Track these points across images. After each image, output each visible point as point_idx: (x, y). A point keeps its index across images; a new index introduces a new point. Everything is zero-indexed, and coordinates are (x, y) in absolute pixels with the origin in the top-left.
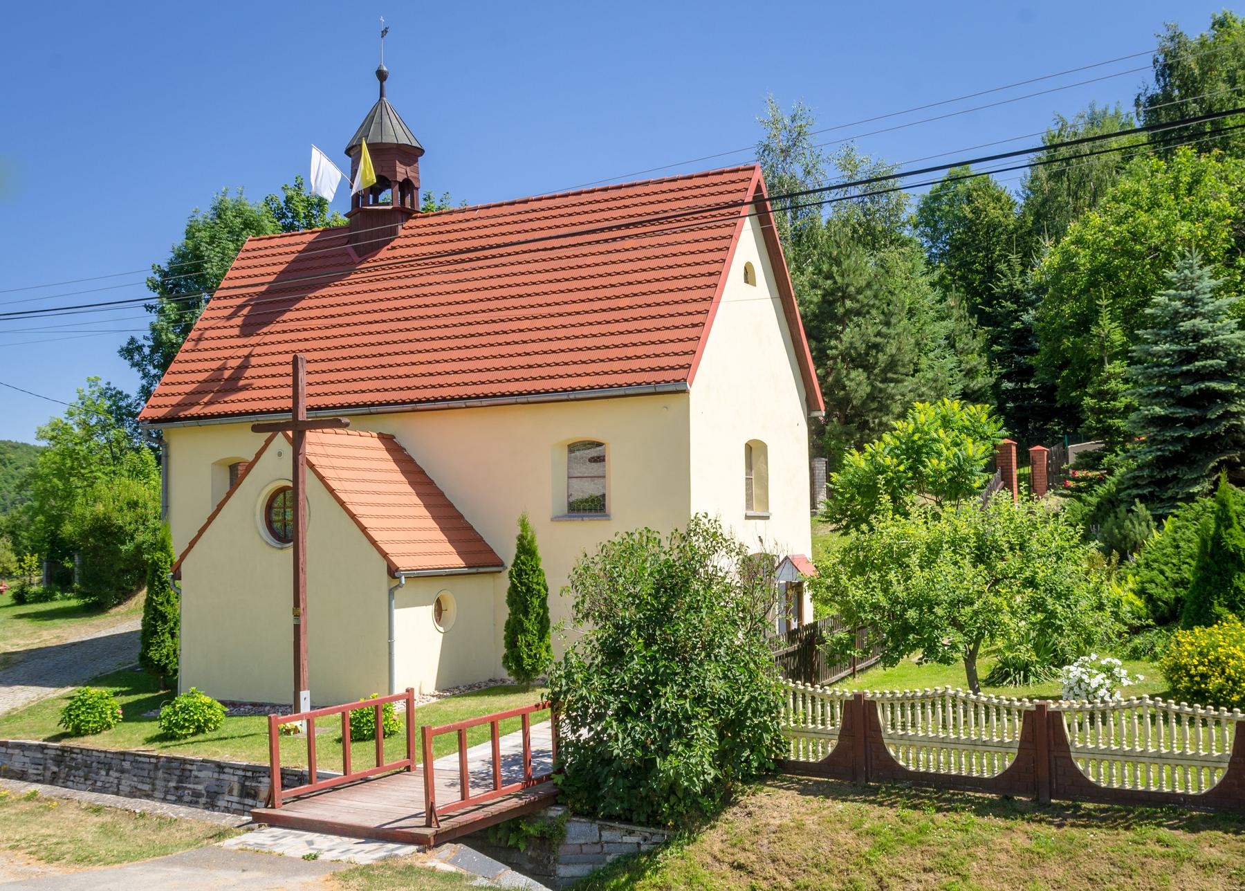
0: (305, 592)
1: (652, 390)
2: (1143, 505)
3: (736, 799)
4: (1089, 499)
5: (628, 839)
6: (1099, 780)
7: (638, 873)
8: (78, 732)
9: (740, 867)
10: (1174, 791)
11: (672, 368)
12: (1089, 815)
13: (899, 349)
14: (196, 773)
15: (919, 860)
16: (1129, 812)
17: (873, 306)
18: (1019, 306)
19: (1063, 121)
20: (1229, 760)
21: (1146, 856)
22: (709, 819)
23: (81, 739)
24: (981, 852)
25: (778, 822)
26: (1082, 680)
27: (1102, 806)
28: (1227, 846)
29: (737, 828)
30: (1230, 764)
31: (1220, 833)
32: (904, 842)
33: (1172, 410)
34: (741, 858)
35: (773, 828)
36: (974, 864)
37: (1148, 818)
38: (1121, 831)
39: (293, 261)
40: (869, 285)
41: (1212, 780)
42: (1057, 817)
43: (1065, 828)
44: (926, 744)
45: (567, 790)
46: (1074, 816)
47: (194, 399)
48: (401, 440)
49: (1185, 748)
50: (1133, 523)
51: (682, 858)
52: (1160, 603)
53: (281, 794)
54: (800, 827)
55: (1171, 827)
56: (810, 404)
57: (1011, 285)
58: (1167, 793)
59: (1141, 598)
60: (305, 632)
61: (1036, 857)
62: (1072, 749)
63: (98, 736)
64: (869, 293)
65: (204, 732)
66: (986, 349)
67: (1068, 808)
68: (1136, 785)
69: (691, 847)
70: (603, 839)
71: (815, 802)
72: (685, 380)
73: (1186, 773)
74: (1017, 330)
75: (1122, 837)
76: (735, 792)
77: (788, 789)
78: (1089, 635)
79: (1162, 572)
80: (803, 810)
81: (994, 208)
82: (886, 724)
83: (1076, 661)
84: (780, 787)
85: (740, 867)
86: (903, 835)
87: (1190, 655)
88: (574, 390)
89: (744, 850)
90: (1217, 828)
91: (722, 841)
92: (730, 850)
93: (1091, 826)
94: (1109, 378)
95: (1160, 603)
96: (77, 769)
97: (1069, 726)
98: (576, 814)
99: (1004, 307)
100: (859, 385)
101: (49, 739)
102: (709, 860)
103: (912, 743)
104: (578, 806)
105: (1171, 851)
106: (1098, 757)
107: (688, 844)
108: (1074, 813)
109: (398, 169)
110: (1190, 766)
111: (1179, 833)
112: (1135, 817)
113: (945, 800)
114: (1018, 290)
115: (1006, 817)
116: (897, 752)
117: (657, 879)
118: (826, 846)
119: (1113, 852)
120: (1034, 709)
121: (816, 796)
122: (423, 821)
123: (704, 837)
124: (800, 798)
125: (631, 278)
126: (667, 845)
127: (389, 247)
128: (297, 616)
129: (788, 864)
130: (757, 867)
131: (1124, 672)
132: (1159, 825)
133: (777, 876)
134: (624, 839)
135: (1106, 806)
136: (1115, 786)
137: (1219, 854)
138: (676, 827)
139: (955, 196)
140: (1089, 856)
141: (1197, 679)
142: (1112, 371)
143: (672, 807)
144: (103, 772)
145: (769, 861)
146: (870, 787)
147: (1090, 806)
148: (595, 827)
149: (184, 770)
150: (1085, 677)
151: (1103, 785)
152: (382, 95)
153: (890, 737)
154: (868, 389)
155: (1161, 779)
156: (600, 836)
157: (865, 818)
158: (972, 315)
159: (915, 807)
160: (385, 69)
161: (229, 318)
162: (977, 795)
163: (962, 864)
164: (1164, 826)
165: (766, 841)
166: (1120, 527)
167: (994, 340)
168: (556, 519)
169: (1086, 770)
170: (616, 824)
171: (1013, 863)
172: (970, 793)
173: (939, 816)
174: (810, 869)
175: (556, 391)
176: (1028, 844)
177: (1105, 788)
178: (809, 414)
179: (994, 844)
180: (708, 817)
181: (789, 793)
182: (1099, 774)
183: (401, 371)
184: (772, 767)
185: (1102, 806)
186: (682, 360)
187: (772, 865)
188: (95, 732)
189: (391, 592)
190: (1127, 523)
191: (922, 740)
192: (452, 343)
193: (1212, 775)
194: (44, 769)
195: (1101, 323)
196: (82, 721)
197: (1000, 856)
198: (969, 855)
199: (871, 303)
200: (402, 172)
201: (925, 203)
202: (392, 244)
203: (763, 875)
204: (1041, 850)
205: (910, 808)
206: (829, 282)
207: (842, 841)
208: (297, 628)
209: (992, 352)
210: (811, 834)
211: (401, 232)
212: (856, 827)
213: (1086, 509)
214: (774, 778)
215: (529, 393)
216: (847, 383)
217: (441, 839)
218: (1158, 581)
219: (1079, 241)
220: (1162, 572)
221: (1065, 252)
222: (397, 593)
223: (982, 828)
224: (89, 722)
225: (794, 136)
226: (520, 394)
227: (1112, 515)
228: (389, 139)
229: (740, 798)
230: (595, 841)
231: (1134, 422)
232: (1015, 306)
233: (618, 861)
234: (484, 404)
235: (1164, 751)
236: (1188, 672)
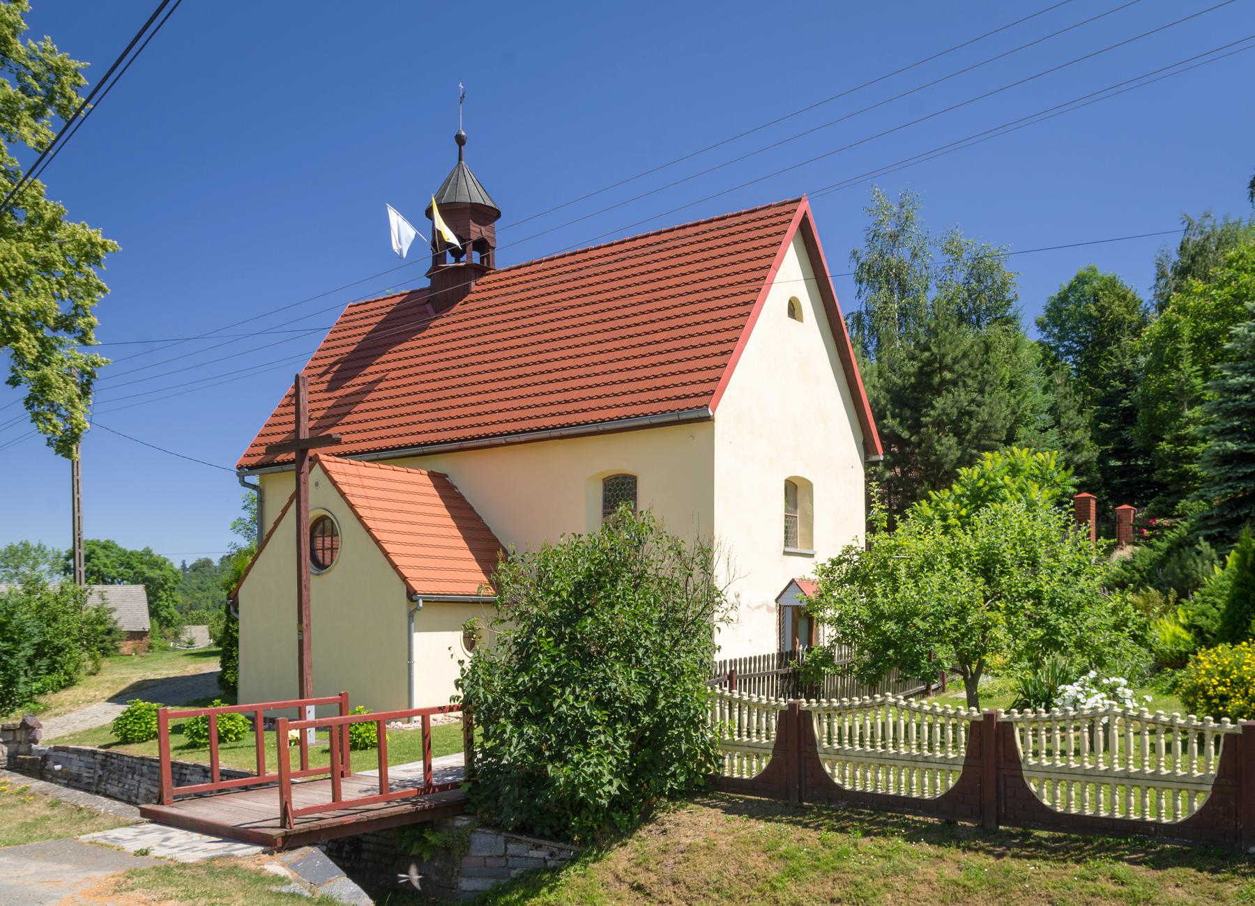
0: (309, 608)
1: (676, 418)
2: (1207, 543)
3: (655, 815)
4: (1159, 544)
5: (534, 853)
6: (1054, 804)
7: (533, 888)
8: (126, 741)
9: (639, 888)
10: (1143, 819)
11: (697, 395)
12: (1038, 845)
13: (991, 415)
14: (188, 777)
15: (828, 889)
16: (1088, 842)
17: (969, 375)
18: (1128, 386)
19: (1188, 218)
20: (1212, 781)
21: (1093, 895)
22: (622, 835)
23: (126, 747)
24: (899, 883)
25: (688, 841)
26: (1078, 700)
27: (1057, 834)
28: (1199, 886)
29: (647, 846)
30: (1214, 786)
31: (1192, 871)
32: (817, 867)
33: (1246, 445)
34: (642, 878)
35: (682, 847)
36: (889, 896)
37: (1107, 850)
38: (1070, 864)
40: (965, 355)
41: (1191, 806)
42: (1000, 846)
43: (1005, 859)
44: (864, 759)
45: (474, 800)
46: (1021, 845)
48: (455, 479)
49: (1159, 766)
50: (1195, 562)
51: (584, 876)
52: (1208, 635)
53: (170, 789)
54: (710, 848)
55: (1131, 862)
56: (867, 448)
57: (1121, 366)
58: (1134, 821)
59: (1189, 632)
60: (309, 648)
61: (961, 890)
62: (1024, 767)
63: (142, 745)
64: (966, 363)
65: (225, 742)
66: (1094, 425)
67: (1015, 836)
68: (1098, 810)
69: (596, 865)
70: (509, 852)
71: (737, 822)
72: (707, 406)
73: (1159, 798)
74: (1125, 409)
75: (1070, 871)
76: (656, 808)
77: (715, 807)
78: (1101, 655)
79: (1214, 605)
80: (721, 829)
81: (1119, 306)
82: (821, 738)
83: (1077, 681)
84: (704, 805)
85: (639, 888)
86: (819, 860)
87: (1209, 674)
88: (603, 421)
89: (648, 870)
90: (1190, 864)
91: (629, 860)
92: (634, 870)
93: (1035, 857)
94: (1187, 423)
95: (1208, 635)
96: (114, 773)
97: (1022, 738)
98: (485, 825)
99: (1112, 386)
100: (949, 448)
101: (100, 747)
102: (610, 878)
103: (848, 758)
104: (486, 816)
105: (1125, 889)
106: (1054, 776)
107: (594, 862)
108: (1022, 841)
109: (472, 228)
110: (1165, 788)
111: (1141, 871)
112: (1092, 849)
113: (878, 823)
114: (1128, 371)
115: (940, 844)
116: (833, 768)
117: (551, 898)
118: (732, 869)
119: (1054, 888)
120: (981, 719)
121: (740, 814)
122: (278, 823)
123: (612, 855)
124: (723, 817)
125: (670, 313)
126: (573, 861)
128: (301, 631)
129: (688, 887)
130: (655, 889)
131: (1129, 692)
132: (1118, 859)
133: (673, 899)
134: (535, 853)
135: (1061, 834)
136: (1074, 811)
137: (1185, 896)
138: (583, 842)
139: (1083, 296)
140: (1025, 892)
141: (1216, 701)
142: (1191, 415)
143: (581, 822)
144: (130, 776)
145: (670, 883)
146: (997, 832)
147: (1044, 834)
148: (501, 839)
149: (181, 774)
150: (1080, 696)
151: (1059, 810)
152: (460, 159)
153: (825, 751)
154: (959, 454)
155: (1143, 806)
156: (506, 849)
157: (783, 840)
158: (1077, 392)
159: (842, 830)
160: (463, 133)
161: (321, 375)
162: (917, 818)
163: (875, 895)
164: (1123, 860)
165: (672, 861)
166: (1183, 567)
167: (1100, 418)
169: (1039, 792)
170: (524, 838)
171: (934, 897)
172: (910, 817)
173: (865, 842)
174: (710, 894)
175: (587, 423)
176: (960, 877)
177: (1061, 814)
178: (866, 457)
179: (917, 873)
180: (621, 834)
181: (712, 811)
182: (1054, 797)
183: (453, 413)
184: (702, 783)
185: (1057, 834)
186: (706, 388)
187: (671, 888)
188: (140, 740)
189: (411, 616)
190: (1190, 562)
191: (858, 755)
192: (501, 385)
193: (1191, 800)
194: (95, 772)
195: (1181, 366)
196: (129, 730)
197: (921, 888)
198: (885, 885)
199: (967, 372)
200: (476, 231)
201: (1053, 304)
202: (465, 300)
203: (659, 898)
204: (969, 883)
205: (836, 830)
206: (927, 354)
207: (751, 863)
208: (301, 643)
209: (1101, 430)
210: (720, 855)
211: (474, 288)
212: (769, 850)
213: (1155, 554)
214: (705, 795)
215: (563, 426)
216: (938, 448)
217: (291, 842)
218: (1209, 614)
219: (1182, 310)
220: (1214, 605)
221: (1168, 322)
222: (417, 615)
223: (909, 856)
224: (135, 731)
225: (903, 220)
226: (555, 428)
227: (1175, 555)
228: (464, 198)
229: (659, 815)
230: (499, 854)
231: (1207, 462)
232: (1124, 386)
233: (522, 876)
235: (1133, 769)
236: (1205, 693)
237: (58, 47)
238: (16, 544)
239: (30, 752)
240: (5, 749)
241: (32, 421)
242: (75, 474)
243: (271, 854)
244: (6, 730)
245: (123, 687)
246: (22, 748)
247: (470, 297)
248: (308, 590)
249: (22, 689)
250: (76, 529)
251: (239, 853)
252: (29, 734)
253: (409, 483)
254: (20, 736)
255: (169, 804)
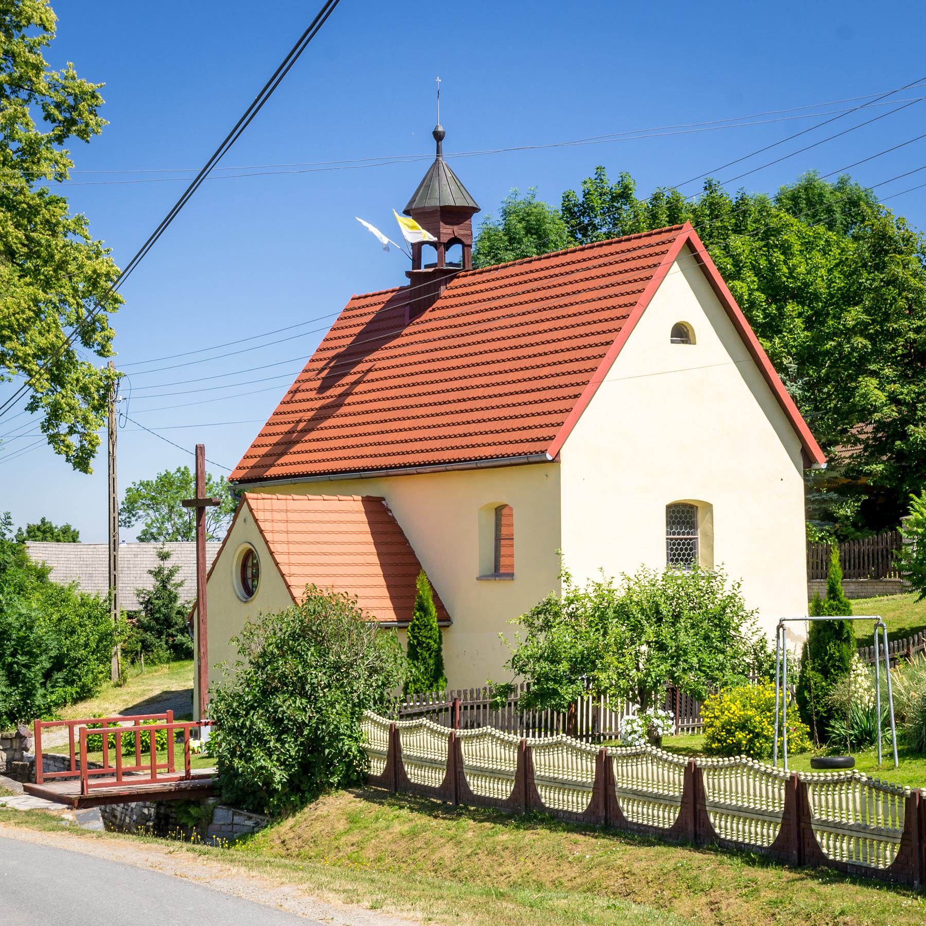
1: (525, 460)
39: (370, 322)
47: (269, 461)
48: (391, 503)
127: (431, 309)
168: (482, 578)
202: (434, 306)
224: (95, 741)
234: (428, 470)
237: (78, 73)
238: (173, 471)
239: (22, 758)
240: (4, 755)
241: (49, 443)
242: (111, 472)
243: (72, 809)
244: (5, 739)
245: (138, 700)
246: (17, 756)
247: (439, 303)
248: (205, 624)
249: (39, 700)
250: (112, 531)
251: (52, 808)
252: (21, 743)
253: (337, 512)
254: (16, 744)
255: (40, 784)
